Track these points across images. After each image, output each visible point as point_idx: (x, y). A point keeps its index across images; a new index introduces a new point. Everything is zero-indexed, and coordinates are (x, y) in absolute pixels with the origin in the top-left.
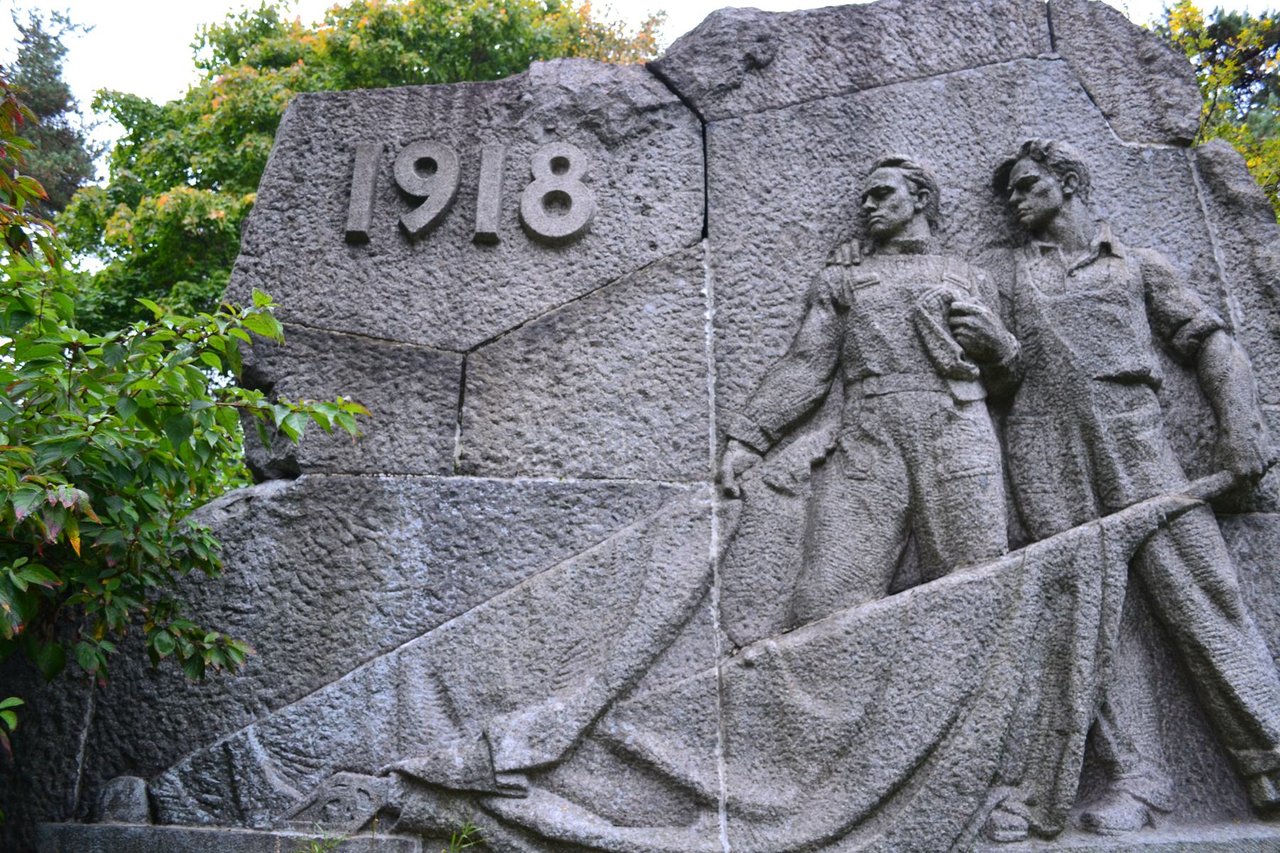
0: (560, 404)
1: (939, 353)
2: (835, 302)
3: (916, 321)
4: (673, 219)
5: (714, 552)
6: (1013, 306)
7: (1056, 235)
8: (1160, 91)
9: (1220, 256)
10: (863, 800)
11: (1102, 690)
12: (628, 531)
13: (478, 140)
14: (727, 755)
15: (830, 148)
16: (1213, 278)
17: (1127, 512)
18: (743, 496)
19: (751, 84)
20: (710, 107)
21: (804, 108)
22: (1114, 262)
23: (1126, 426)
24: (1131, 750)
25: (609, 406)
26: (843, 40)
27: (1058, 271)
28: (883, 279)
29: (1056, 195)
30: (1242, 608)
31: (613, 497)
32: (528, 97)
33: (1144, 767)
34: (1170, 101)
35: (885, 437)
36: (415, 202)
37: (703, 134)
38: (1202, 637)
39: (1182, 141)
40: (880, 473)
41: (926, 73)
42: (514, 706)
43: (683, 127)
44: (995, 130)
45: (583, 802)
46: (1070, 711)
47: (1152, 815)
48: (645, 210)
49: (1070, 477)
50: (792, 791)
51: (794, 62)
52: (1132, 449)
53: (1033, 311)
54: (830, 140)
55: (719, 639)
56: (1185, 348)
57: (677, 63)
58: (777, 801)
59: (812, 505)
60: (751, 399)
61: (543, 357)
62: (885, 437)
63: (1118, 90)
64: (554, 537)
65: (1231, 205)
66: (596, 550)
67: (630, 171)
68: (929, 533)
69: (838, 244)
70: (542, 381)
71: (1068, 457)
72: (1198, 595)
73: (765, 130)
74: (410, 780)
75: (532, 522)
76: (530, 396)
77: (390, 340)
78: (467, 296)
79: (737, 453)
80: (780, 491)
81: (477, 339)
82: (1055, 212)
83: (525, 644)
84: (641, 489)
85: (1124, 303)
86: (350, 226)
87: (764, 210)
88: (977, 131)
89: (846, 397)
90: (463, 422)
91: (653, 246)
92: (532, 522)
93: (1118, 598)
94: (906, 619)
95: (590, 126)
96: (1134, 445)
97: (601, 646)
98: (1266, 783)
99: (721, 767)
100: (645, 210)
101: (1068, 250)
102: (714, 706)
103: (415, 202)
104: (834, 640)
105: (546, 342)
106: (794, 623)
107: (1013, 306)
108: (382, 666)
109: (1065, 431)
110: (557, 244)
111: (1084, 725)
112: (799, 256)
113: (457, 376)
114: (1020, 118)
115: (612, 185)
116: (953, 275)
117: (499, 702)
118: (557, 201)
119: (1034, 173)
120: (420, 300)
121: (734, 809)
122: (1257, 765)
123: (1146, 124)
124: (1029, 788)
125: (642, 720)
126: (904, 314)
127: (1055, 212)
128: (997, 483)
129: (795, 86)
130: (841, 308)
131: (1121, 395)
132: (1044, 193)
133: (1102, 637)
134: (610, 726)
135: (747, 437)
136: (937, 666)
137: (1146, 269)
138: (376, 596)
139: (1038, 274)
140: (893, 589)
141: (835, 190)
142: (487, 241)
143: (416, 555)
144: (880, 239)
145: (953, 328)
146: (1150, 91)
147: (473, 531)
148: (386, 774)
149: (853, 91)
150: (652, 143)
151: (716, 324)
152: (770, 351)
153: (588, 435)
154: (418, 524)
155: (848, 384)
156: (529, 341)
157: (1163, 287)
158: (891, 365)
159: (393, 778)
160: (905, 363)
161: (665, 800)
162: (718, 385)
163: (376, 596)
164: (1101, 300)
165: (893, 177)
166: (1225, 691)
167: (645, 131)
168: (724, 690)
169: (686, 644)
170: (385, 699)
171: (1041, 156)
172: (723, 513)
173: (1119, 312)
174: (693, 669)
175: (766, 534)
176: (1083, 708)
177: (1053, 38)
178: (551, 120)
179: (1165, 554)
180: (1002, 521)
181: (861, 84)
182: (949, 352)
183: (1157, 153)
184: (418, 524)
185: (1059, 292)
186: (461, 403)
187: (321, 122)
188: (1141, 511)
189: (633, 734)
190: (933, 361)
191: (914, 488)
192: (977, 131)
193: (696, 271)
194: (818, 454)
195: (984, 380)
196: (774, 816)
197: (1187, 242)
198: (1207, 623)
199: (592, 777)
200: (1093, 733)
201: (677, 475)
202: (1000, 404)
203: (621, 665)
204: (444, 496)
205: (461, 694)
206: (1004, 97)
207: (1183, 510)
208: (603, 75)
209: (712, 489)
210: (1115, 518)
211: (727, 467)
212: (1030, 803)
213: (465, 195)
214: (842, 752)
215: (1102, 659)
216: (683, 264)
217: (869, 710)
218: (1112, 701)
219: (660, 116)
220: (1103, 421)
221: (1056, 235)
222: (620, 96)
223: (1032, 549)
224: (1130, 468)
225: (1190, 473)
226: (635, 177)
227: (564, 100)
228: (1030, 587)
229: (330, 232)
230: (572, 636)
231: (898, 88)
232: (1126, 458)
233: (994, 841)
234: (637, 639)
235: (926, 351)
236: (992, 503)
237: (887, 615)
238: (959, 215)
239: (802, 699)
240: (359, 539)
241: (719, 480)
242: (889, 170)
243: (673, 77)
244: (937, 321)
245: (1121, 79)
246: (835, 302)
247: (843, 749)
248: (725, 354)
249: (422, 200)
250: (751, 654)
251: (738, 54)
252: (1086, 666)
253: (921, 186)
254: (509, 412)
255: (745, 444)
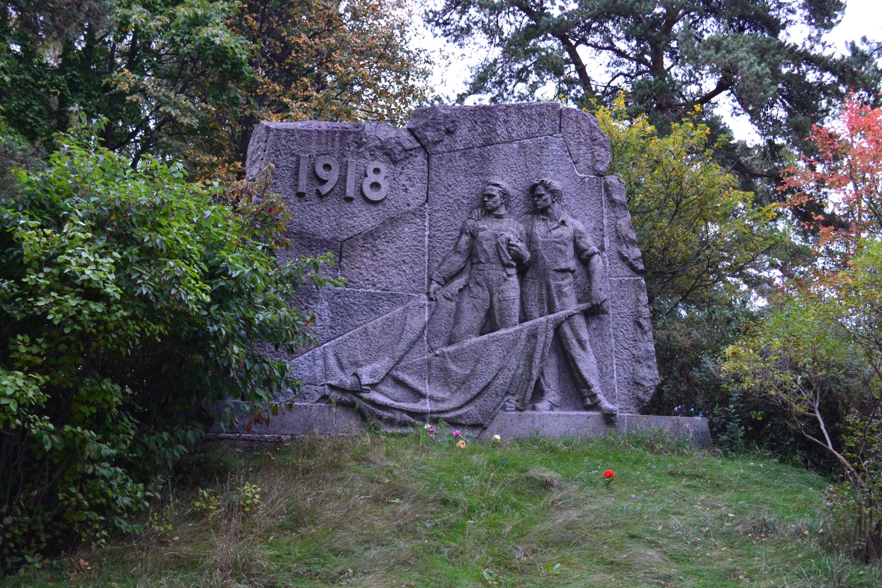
0: (375, 263)
1: (504, 258)
2: (471, 234)
3: (498, 245)
4: (416, 195)
5: (426, 319)
6: (530, 239)
7: (548, 215)
8: (596, 153)
9: (605, 221)
10: (469, 397)
11: (542, 368)
12: (399, 309)
13: (345, 156)
14: (429, 382)
15: (473, 170)
16: (601, 230)
17: (556, 314)
18: (436, 300)
19: (447, 140)
20: (432, 149)
21: (466, 152)
22: (565, 228)
23: (560, 286)
24: (549, 387)
25: (392, 265)
26: (482, 123)
27: (546, 229)
28: (487, 228)
29: (550, 201)
30: (588, 345)
31: (393, 299)
32: (364, 140)
33: (553, 392)
34: (598, 159)
35: (484, 284)
36: (323, 182)
37: (428, 160)
38: (574, 354)
39: (600, 175)
40: (481, 296)
41: (511, 140)
42: (362, 366)
43: (420, 158)
44: (534, 166)
45: (386, 395)
46: (531, 374)
47: (553, 407)
48: (406, 190)
49: (541, 301)
50: (448, 394)
51: (463, 131)
52: (561, 294)
53: (536, 243)
54: (474, 167)
55: (427, 347)
56: (584, 258)
57: (420, 130)
58: (444, 396)
59: (458, 305)
60: (440, 265)
61: (369, 245)
62: (484, 284)
63: (581, 152)
64: (373, 310)
65: (613, 202)
66: (387, 316)
67: (401, 174)
68: (494, 317)
69: (473, 209)
70: (369, 254)
71: (541, 294)
72: (574, 341)
73: (451, 161)
74: (331, 387)
75: (366, 305)
76: (365, 260)
77: (314, 235)
78: (342, 220)
79: (435, 285)
80: (448, 299)
81: (346, 237)
82: (549, 207)
83: (365, 346)
84: (402, 295)
85: (566, 245)
86: (300, 190)
87: (448, 194)
88: (527, 167)
89: (472, 268)
90: (342, 268)
91: (408, 205)
92: (366, 305)
93: (549, 341)
94: (485, 344)
95: (387, 154)
96: (562, 293)
97: (390, 348)
98: (588, 399)
99: (427, 386)
100: (406, 190)
101: (551, 221)
102: (426, 368)
103: (323, 182)
104: (463, 349)
105: (370, 240)
106: (450, 343)
107: (530, 239)
108: (318, 351)
109: (541, 286)
110: (375, 203)
111: (535, 378)
112: (459, 213)
113: (341, 249)
114: (543, 162)
115: (394, 179)
116: (509, 229)
117: (357, 364)
118: (376, 186)
119: (543, 192)
120: (325, 221)
121: (431, 398)
122: (586, 394)
123: (589, 167)
124: (517, 397)
125: (404, 371)
126: (494, 242)
127: (549, 207)
128: (517, 302)
129: (463, 142)
130: (473, 236)
131: (560, 276)
132: (546, 200)
133: (543, 353)
134: (394, 373)
135: (438, 280)
136: (493, 359)
137: (575, 231)
138: (313, 328)
139: (540, 228)
140: (482, 334)
141: (474, 188)
142: (349, 200)
143: (326, 314)
144: (490, 212)
145: (509, 250)
146: (592, 153)
147: (346, 307)
148: (323, 385)
149: (484, 146)
150: (409, 163)
151: (429, 237)
152: (447, 248)
153: (384, 275)
154: (327, 304)
155: (472, 264)
156: (364, 239)
157: (580, 238)
158: (488, 260)
159: (326, 387)
160: (493, 260)
161: (410, 395)
162: (429, 260)
163: (313, 328)
164: (558, 243)
165: (495, 191)
166: (579, 371)
167: (408, 158)
168: (429, 363)
169: (417, 348)
170: (320, 362)
171: (547, 187)
172: (429, 306)
173: (563, 247)
174: (417, 358)
175: (443, 313)
176: (535, 373)
177: (561, 127)
178: (373, 150)
179: (567, 329)
180: (518, 314)
181: (488, 143)
182: (507, 258)
183: (590, 179)
184: (327, 304)
185: (545, 238)
186: (340, 261)
187: (284, 142)
188: (560, 314)
189: (401, 375)
190: (502, 261)
191: (491, 302)
192: (527, 167)
193: (423, 216)
194: (461, 287)
195: (517, 267)
196: (443, 400)
197: (594, 216)
198: (576, 350)
199: (389, 389)
200: (538, 382)
201: (413, 291)
202: (522, 273)
203: (398, 354)
204: (336, 294)
205: (345, 361)
206: (539, 153)
207: (574, 315)
208: (392, 134)
209: (426, 297)
210: (552, 316)
211: (432, 290)
212: (517, 401)
213: (343, 179)
214: (464, 383)
215: (543, 358)
216: (419, 213)
217: (472, 371)
218: (545, 372)
219: (413, 152)
220: (553, 284)
221: (548, 215)
222: (399, 144)
223: (526, 324)
224: (559, 300)
225: (579, 301)
226: (403, 176)
227: (377, 142)
228: (523, 336)
229: (290, 190)
230: (380, 344)
231: (501, 146)
232: (559, 296)
233: (505, 411)
234: (402, 346)
235: (500, 257)
236: (516, 308)
237: (480, 342)
238: (516, 201)
239: (453, 367)
240: (306, 308)
241: (428, 294)
242: (495, 188)
243: (419, 136)
244: (504, 247)
245: (583, 148)
246: (471, 234)
247: (464, 382)
248: (432, 248)
249: (326, 181)
250: (438, 352)
251: (443, 128)
252: (537, 361)
253: (505, 194)
254: (357, 265)
255: (437, 282)
